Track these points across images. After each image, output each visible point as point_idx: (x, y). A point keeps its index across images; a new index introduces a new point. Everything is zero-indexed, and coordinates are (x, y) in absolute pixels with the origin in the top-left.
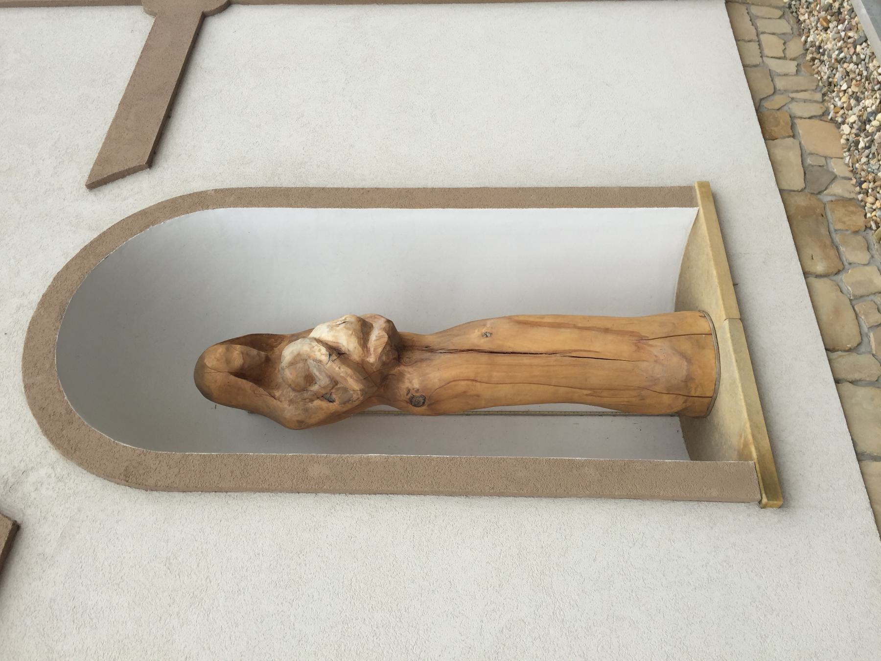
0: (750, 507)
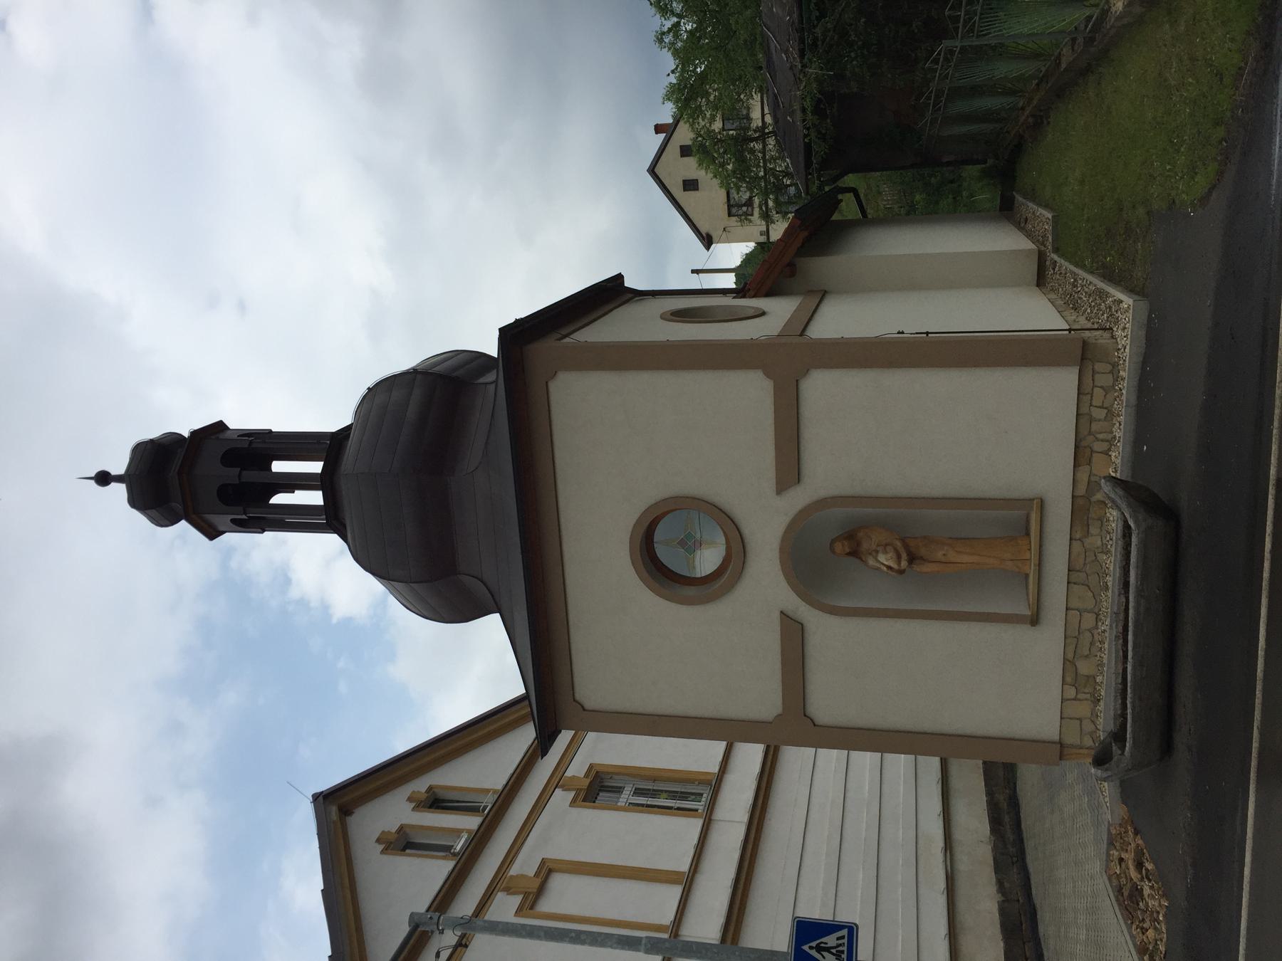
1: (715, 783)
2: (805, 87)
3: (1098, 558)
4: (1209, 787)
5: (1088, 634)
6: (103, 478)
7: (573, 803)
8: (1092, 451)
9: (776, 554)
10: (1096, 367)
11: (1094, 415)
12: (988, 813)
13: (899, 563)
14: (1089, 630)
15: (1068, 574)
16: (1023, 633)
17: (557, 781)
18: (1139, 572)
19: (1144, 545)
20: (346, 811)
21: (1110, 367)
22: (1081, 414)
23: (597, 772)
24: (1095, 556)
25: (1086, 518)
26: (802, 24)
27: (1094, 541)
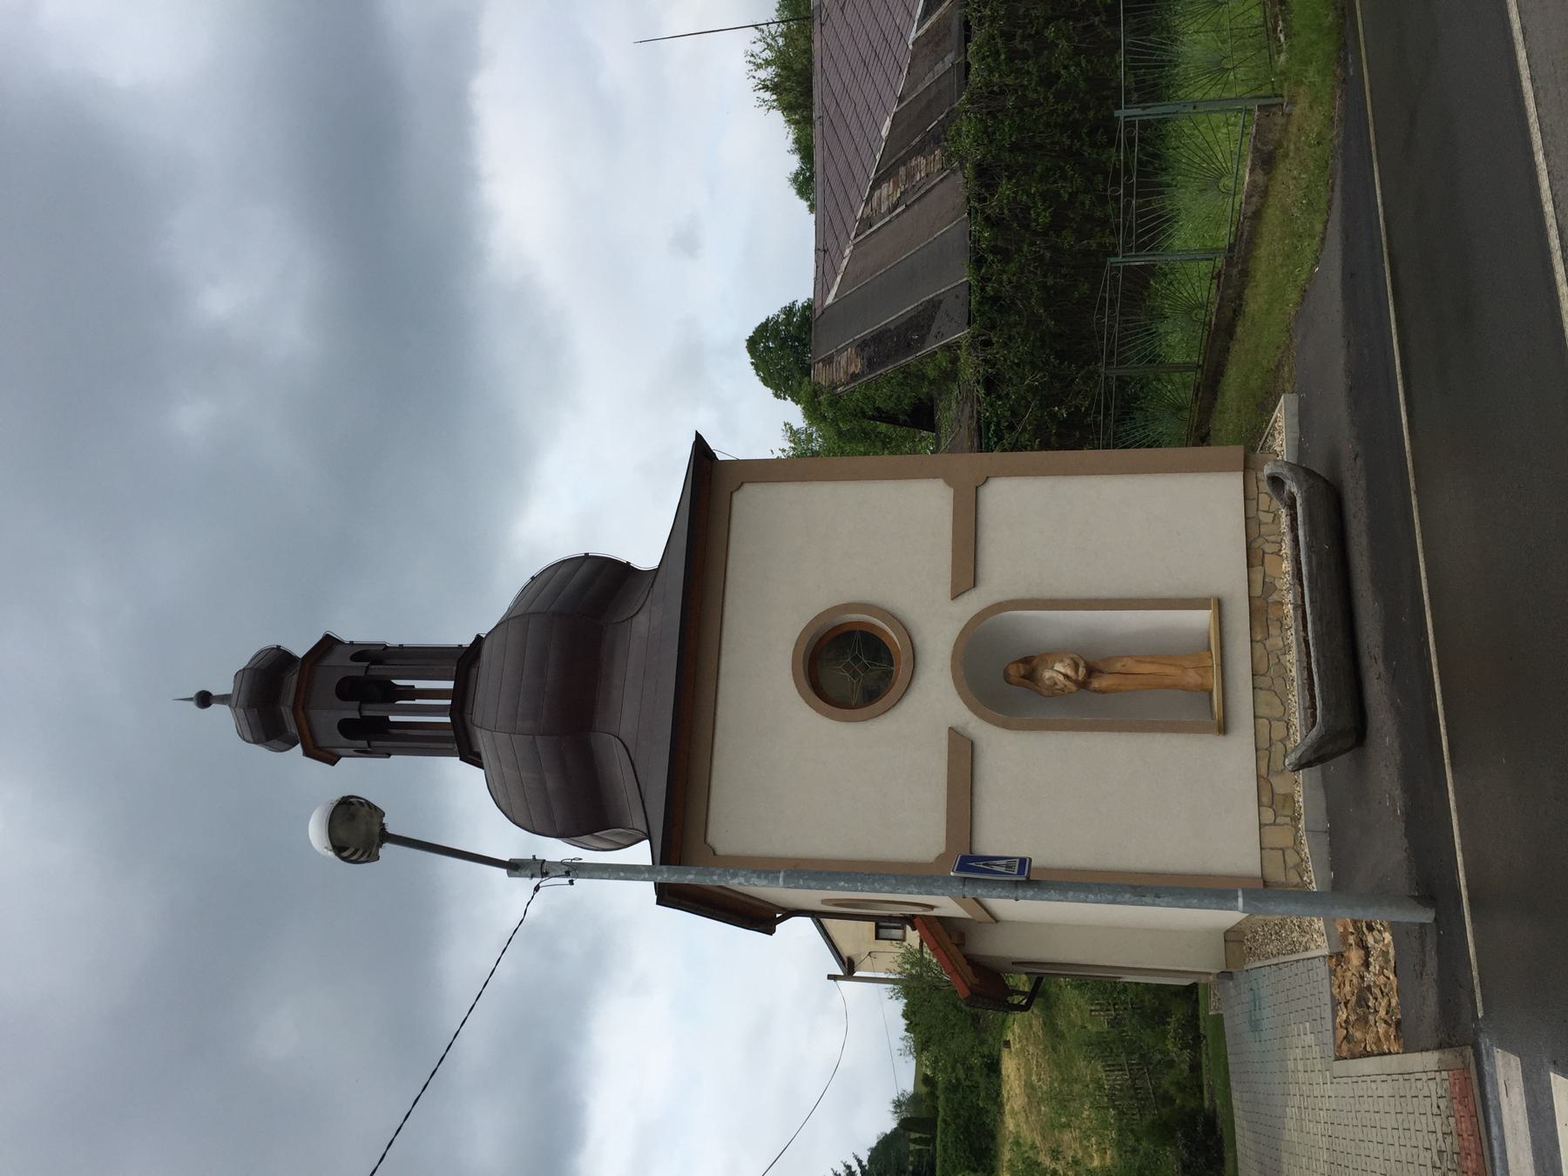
0: (1333, 712)
3: (1282, 661)
5: (1280, 746)
6: (204, 699)
8: (1264, 553)
9: (948, 663)
11: (1261, 518)
13: (1077, 672)
14: (1281, 741)
22: (1254, 597)
24: (1278, 658)
27: (1275, 642)
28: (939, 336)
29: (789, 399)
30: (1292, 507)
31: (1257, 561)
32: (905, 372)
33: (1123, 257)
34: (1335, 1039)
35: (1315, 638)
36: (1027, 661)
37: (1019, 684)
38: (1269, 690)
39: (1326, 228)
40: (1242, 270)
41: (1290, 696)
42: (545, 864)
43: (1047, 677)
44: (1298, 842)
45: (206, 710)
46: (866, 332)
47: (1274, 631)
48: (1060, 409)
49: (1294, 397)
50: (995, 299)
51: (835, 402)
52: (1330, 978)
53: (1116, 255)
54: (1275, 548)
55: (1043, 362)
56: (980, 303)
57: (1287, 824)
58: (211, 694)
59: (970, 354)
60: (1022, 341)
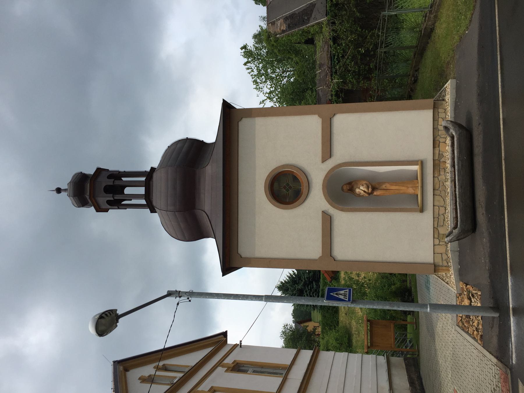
1: (289, 369)
2: (332, 87)
3: (444, 184)
4: (489, 216)
6: (59, 190)
7: (226, 371)
8: (440, 142)
9: (321, 187)
10: (436, 159)
12: (408, 381)
13: (368, 190)
15: (433, 192)
16: (417, 216)
17: (220, 363)
18: (458, 151)
19: (459, 139)
20: (126, 370)
21: (444, 111)
22: (435, 128)
23: (237, 363)
24: (443, 183)
25: (439, 168)
26: (332, 65)
27: (442, 177)
28: (315, 19)
29: (261, 4)
30: (452, 138)
31: (437, 146)
32: (303, 31)
33: (388, 12)
34: (457, 320)
35: (459, 194)
36: (350, 183)
37: (347, 192)
38: (439, 195)
39: (472, 17)
40: (435, 15)
41: (447, 198)
42: (180, 292)
43: (357, 191)
44: (447, 251)
45: (60, 194)
46: (287, 13)
47: (442, 173)
48: (361, 49)
49: (454, 81)
50: (337, 5)
51: (277, 40)
52: (456, 299)
53: (385, 11)
54: (444, 140)
55: (355, 30)
56: (330, 7)
57: (444, 245)
58: (61, 189)
59: (327, 27)
60: (347, 22)
